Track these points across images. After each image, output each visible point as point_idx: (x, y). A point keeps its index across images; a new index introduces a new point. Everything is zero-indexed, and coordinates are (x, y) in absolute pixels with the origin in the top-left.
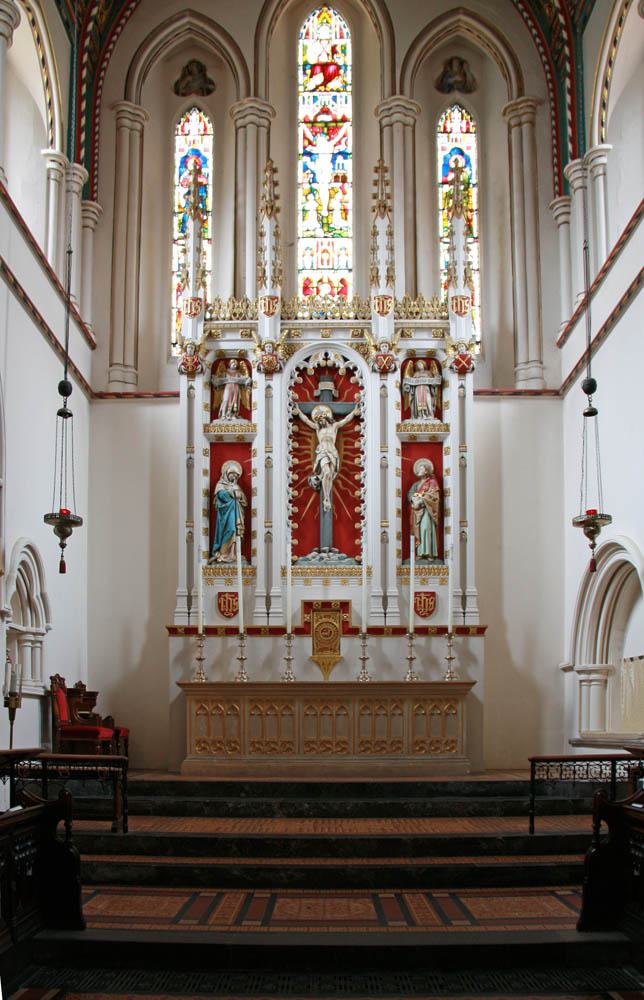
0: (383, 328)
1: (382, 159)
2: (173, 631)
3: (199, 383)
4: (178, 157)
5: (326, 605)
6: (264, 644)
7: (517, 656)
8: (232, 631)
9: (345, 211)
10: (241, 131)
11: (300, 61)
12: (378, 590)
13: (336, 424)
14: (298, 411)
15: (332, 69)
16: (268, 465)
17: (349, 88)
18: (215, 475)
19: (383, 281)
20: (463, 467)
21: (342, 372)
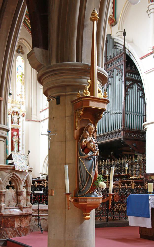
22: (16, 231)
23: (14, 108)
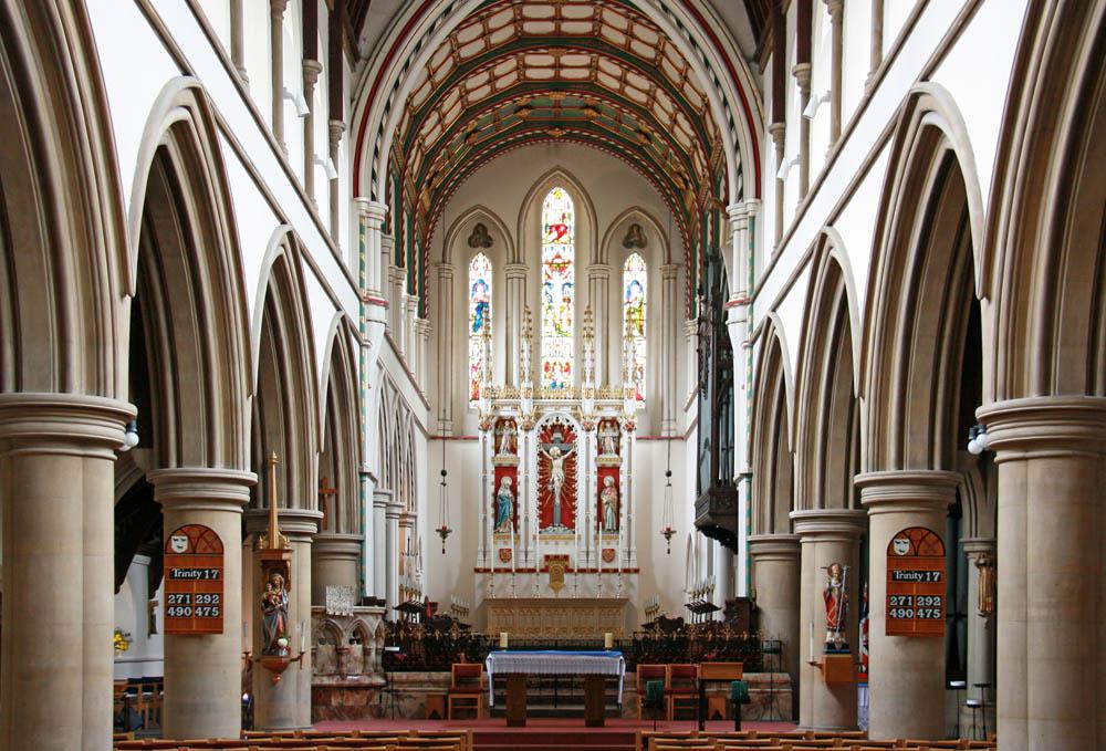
0: (588, 406)
1: (589, 307)
2: (477, 571)
3: (489, 435)
4: (471, 284)
5: (557, 557)
6: (525, 577)
7: (660, 585)
8: (508, 571)
9: (570, 321)
10: (509, 281)
11: (544, 224)
12: (584, 549)
13: (563, 457)
14: (542, 449)
15: (562, 229)
16: (527, 480)
17: (573, 242)
18: (498, 485)
19: (588, 379)
20: (630, 482)
21: (566, 428)
22: (332, 711)
23: (605, 409)
